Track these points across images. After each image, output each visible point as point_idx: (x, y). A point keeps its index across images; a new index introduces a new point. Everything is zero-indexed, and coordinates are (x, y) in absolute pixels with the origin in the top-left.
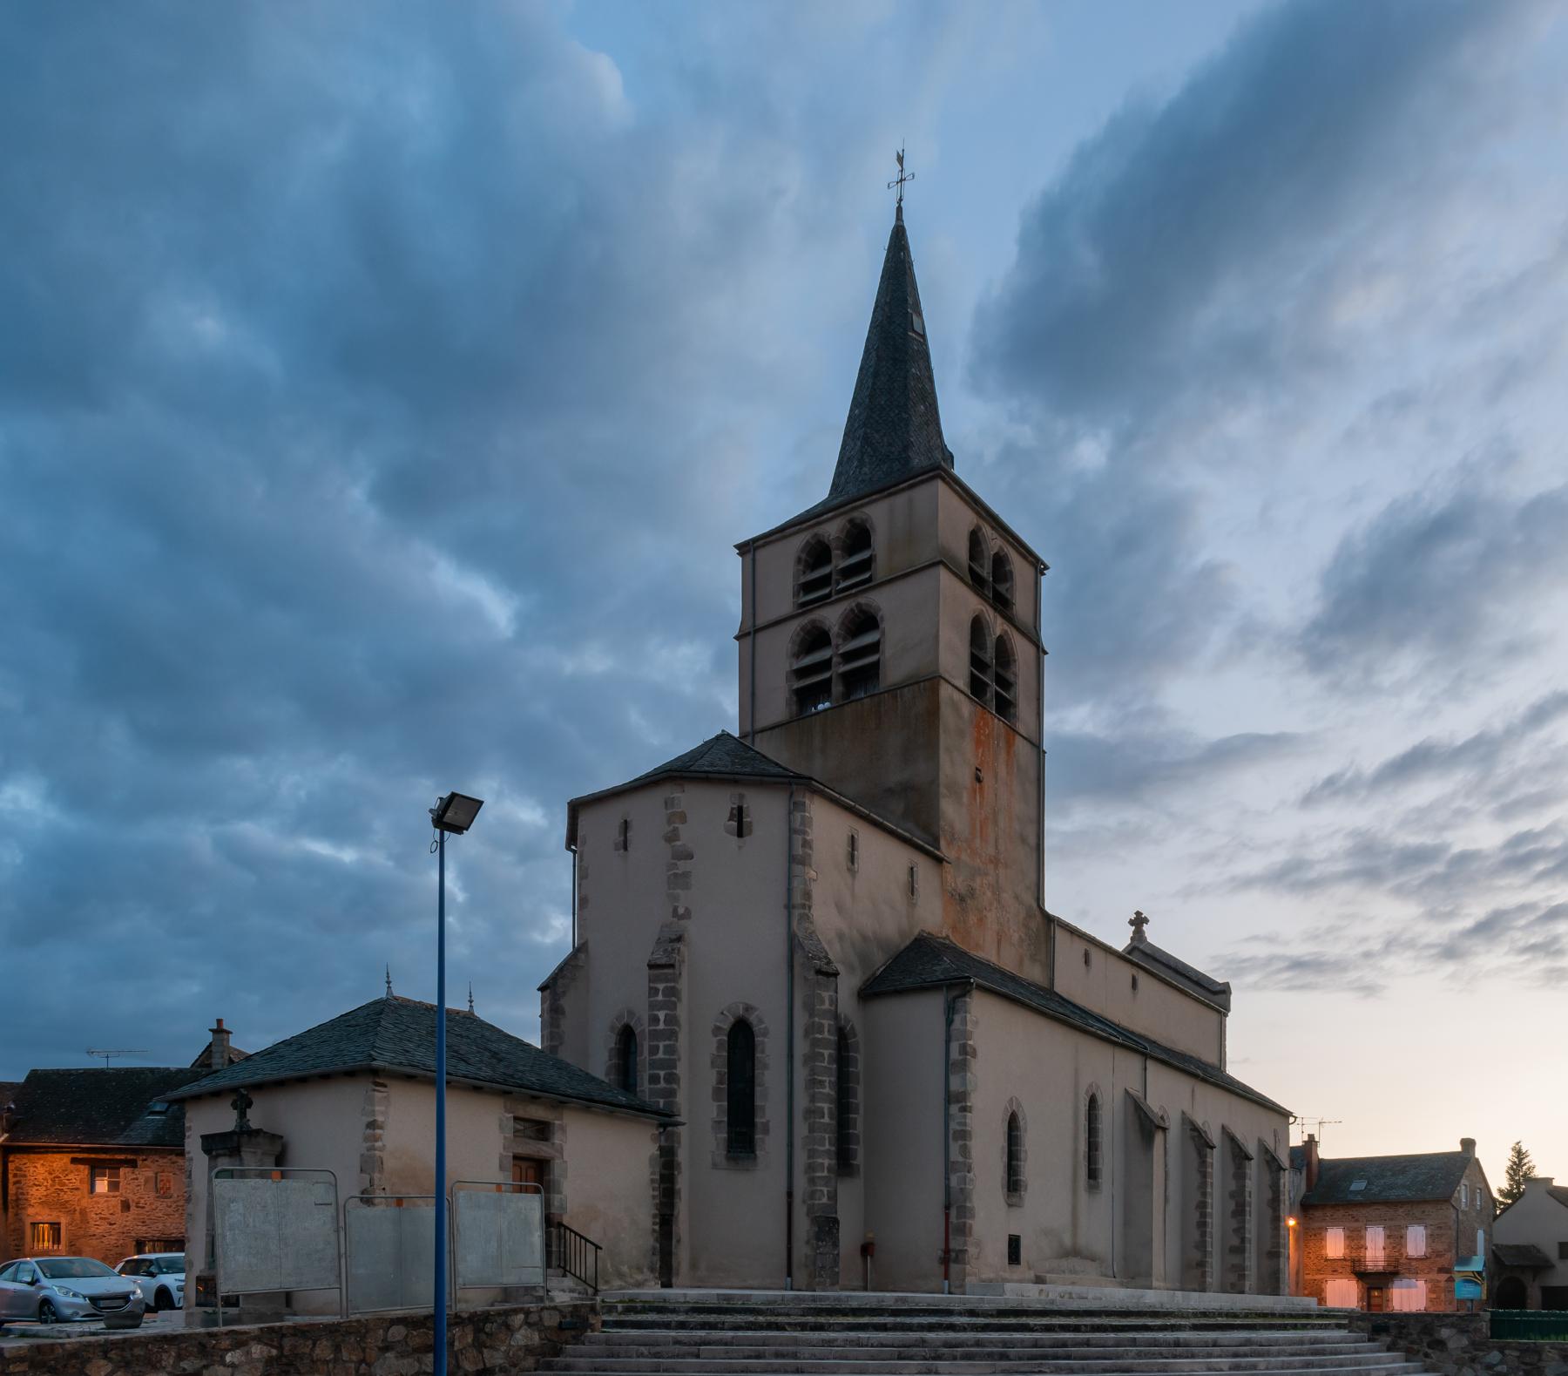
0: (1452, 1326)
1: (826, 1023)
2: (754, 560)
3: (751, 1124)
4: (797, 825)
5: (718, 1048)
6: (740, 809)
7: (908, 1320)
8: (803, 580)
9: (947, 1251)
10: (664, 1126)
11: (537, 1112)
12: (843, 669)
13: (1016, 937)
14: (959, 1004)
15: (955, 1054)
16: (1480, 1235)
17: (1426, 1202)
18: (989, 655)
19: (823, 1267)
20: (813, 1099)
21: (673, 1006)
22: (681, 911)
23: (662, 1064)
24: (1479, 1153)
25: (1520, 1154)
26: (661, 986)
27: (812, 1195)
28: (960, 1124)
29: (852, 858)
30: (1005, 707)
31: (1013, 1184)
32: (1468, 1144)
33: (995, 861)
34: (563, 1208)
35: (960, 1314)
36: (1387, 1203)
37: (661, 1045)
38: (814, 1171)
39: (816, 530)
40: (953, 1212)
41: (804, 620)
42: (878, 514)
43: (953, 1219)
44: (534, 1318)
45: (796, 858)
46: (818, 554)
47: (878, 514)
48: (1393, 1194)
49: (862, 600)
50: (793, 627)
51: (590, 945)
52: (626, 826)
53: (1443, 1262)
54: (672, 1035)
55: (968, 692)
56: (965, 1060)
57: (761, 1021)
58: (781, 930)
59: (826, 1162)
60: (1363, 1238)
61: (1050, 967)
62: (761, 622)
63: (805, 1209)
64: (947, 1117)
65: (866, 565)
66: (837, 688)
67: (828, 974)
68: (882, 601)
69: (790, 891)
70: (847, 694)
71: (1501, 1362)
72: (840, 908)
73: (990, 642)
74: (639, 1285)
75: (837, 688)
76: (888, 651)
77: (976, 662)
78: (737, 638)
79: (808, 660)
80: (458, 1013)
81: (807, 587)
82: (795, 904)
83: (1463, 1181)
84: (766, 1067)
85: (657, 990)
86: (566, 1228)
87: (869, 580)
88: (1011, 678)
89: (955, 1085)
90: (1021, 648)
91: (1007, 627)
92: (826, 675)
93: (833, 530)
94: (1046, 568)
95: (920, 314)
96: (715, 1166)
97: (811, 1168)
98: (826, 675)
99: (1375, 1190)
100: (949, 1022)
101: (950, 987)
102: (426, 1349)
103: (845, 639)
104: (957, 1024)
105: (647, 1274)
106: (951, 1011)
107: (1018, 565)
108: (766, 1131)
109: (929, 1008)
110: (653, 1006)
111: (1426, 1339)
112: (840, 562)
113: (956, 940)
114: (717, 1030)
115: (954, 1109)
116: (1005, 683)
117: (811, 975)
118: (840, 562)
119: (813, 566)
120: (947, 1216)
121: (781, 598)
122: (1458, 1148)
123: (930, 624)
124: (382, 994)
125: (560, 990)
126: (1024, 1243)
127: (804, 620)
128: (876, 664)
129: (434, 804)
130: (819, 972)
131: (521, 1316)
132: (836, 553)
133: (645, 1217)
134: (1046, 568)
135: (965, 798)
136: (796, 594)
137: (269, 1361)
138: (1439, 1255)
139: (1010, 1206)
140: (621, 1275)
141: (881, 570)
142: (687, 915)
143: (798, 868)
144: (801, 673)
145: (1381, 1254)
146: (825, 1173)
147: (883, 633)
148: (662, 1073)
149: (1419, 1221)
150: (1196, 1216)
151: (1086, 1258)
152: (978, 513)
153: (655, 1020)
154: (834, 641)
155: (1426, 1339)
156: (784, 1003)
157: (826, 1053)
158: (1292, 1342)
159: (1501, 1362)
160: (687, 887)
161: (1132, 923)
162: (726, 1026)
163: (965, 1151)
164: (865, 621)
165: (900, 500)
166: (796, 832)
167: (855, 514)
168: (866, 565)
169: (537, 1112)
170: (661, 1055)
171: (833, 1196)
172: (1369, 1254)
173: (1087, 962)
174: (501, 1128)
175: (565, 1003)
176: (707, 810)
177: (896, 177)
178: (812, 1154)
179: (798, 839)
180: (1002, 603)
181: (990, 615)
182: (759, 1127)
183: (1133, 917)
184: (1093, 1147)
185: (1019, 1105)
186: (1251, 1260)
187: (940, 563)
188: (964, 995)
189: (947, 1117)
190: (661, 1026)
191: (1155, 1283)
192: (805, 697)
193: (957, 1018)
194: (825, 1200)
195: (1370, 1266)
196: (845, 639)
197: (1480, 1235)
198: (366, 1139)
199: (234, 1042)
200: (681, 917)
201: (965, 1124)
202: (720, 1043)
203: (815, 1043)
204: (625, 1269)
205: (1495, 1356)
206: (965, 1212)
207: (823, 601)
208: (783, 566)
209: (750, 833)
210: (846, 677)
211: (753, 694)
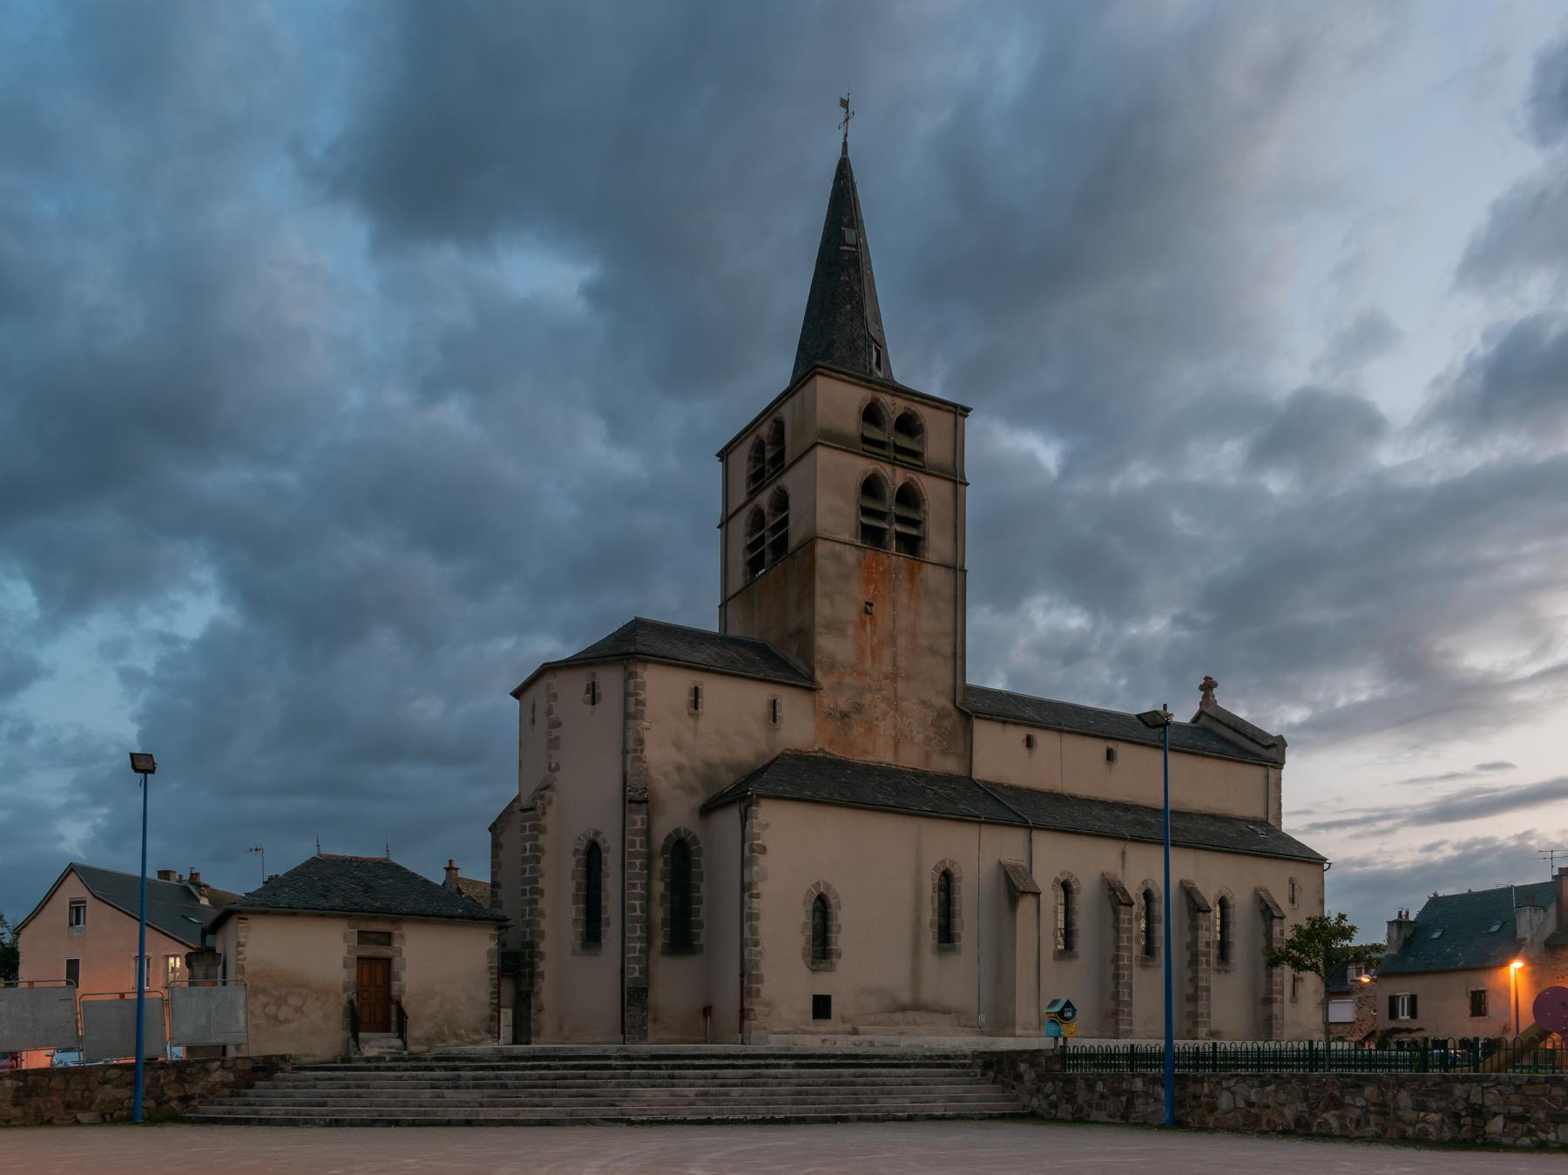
0: (1025, 1061)
1: (638, 839)
4: (631, 689)
10: (500, 928)
12: (899, 528)
13: (920, 738)
19: (633, 1027)
33: (893, 677)
34: (402, 991)
35: (616, 1058)
45: (631, 713)
64: (742, 902)
69: (625, 741)
72: (678, 746)
74: (476, 1043)
82: (631, 748)
90: (932, 489)
93: (765, 430)
100: (743, 828)
105: (484, 1035)
106: (744, 818)
108: (608, 924)
113: (837, 752)
114: (576, 852)
124: (315, 854)
135: (850, 630)
137: (18, 1089)
140: (457, 1036)
142: (557, 768)
143: (631, 722)
150: (1111, 969)
151: (935, 1011)
157: (638, 862)
161: (1201, 688)
162: (582, 848)
174: (345, 939)
175: (503, 840)
187: (817, 444)
189: (742, 902)
191: (1018, 1032)
192: (754, 564)
199: (460, 874)
202: (578, 861)
204: (462, 1032)
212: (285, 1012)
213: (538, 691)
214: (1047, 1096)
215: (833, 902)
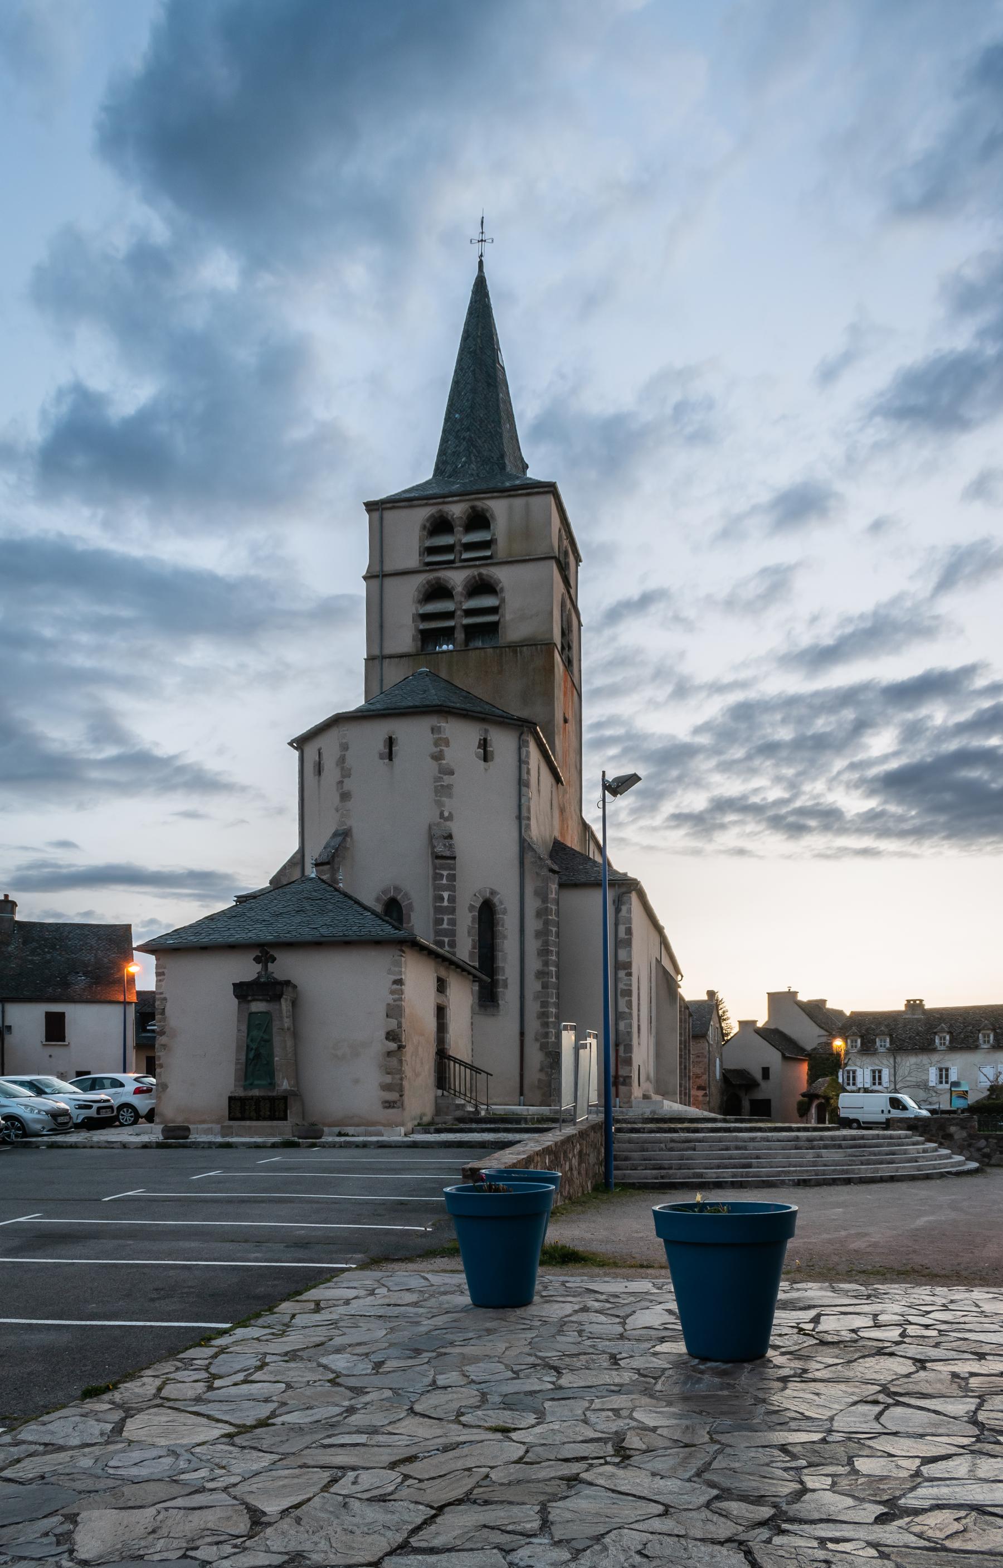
0: (957, 1125)
5: (473, 921)
6: (485, 740)
7: (700, 1125)
8: (428, 543)
12: (467, 621)
14: (625, 898)
22: (446, 814)
32: (711, 994)
37: (446, 918)
39: (440, 507)
40: (621, 1048)
41: (431, 576)
43: (621, 1053)
46: (440, 525)
49: (484, 571)
50: (420, 579)
51: (354, 831)
52: (391, 742)
54: (452, 910)
57: (501, 903)
58: (515, 835)
66: (460, 635)
68: (502, 575)
70: (467, 641)
71: (986, 1147)
76: (509, 615)
78: (365, 578)
79: (431, 608)
82: (522, 818)
85: (442, 876)
93: (457, 510)
104: (624, 912)
108: (506, 986)
111: (941, 1133)
114: (471, 908)
121: (407, 551)
122: (705, 997)
125: (336, 866)
127: (431, 576)
132: (459, 529)
142: (450, 818)
144: (425, 617)
148: (446, 940)
154: (457, 598)
155: (941, 1133)
158: (854, 1138)
159: (986, 1147)
160: (450, 796)
162: (478, 905)
167: (478, 503)
168: (486, 545)
170: (445, 926)
179: (524, 767)
186: (877, 1081)
192: (428, 638)
193: (624, 908)
194: (553, 1039)
198: (392, 992)
200: (447, 819)
202: (473, 918)
205: (982, 1143)
206: (629, 1048)
208: (409, 530)
209: (492, 759)
210: (467, 628)
211: (381, 626)
213: (329, 743)
214: (979, 1150)
215: (499, 908)
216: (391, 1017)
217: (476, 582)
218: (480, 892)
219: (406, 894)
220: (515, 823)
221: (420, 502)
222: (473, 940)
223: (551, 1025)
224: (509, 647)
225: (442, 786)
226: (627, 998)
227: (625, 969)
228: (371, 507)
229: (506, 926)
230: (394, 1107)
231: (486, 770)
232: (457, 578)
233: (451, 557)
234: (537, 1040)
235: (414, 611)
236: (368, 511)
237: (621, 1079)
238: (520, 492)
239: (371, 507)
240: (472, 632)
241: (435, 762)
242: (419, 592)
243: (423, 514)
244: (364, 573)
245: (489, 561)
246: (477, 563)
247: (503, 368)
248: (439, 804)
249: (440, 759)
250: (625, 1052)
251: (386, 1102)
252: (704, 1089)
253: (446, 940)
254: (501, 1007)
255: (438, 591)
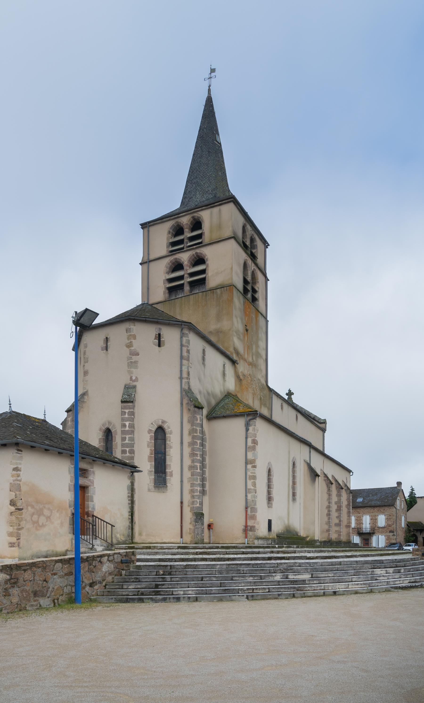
2: (149, 231)
3: (165, 473)
5: (150, 439)
6: (159, 335)
8: (171, 240)
9: (246, 526)
11: (83, 465)
15: (250, 443)
16: (403, 518)
17: (385, 506)
18: (249, 279)
20: (193, 461)
21: (133, 420)
22: (134, 378)
23: (127, 445)
24: (403, 487)
25: (412, 490)
26: (127, 411)
27: (193, 503)
28: (252, 473)
29: (204, 359)
30: (254, 299)
31: (270, 499)
32: (399, 484)
34: (94, 508)
36: (370, 507)
37: (127, 437)
38: (194, 492)
39: (177, 220)
40: (249, 510)
42: (206, 216)
44: (111, 558)
46: (179, 230)
47: (206, 216)
48: (373, 503)
49: (198, 251)
50: (167, 261)
51: (89, 392)
52: (107, 340)
53: (391, 528)
55: (243, 293)
56: (254, 446)
57: (169, 428)
59: (199, 489)
60: (362, 520)
61: (271, 410)
62: (152, 257)
63: (189, 509)
65: (200, 236)
66: (187, 288)
67: (201, 408)
73: (250, 273)
75: (187, 288)
77: (245, 281)
78: (141, 264)
80: (39, 419)
81: (173, 244)
83: (398, 498)
84: (171, 447)
85: (125, 412)
86: (96, 517)
87: (201, 243)
88: (257, 289)
89: (250, 456)
91: (255, 268)
92: (182, 282)
93: (185, 220)
94: (269, 245)
95: (219, 135)
96: (149, 490)
97: (192, 491)
98: (182, 282)
99: (366, 501)
100: (247, 430)
101: (248, 415)
102: (70, 574)
103: (190, 268)
106: (247, 426)
107: (259, 243)
108: (171, 475)
109: (237, 425)
110: (123, 420)
112: (188, 234)
115: (249, 466)
116: (254, 291)
117: (192, 408)
118: (188, 234)
119: (176, 235)
120: (246, 512)
123: (223, 263)
126: (273, 522)
127: (172, 258)
128: (204, 279)
129: (80, 310)
130: (195, 407)
131: (106, 557)
132: (186, 230)
133: (126, 514)
134: (269, 245)
136: (168, 247)
138: (390, 526)
139: (269, 507)
141: (206, 238)
142: (137, 380)
144: (171, 280)
145: (368, 526)
146: (198, 494)
147: (208, 266)
148: (128, 449)
149: (383, 513)
152: (245, 219)
153: (124, 426)
154: (185, 268)
156: (179, 420)
160: (136, 367)
162: (154, 429)
163: (254, 485)
164: (200, 260)
165: (215, 210)
166: (185, 346)
167: (195, 214)
168: (200, 236)
169: (83, 465)
170: (127, 441)
171: (201, 503)
172: (364, 526)
173: (282, 408)
176: (145, 333)
177: (208, 76)
178: (192, 485)
180: (253, 257)
181: (250, 262)
182: (168, 474)
183: (287, 392)
184: (294, 483)
185: (271, 465)
188: (254, 419)
190: (127, 428)
194: (198, 505)
195: (364, 531)
196: (190, 268)
197: (403, 518)
200: (134, 381)
201: (254, 473)
202: (151, 437)
203: (194, 437)
206: (254, 510)
207: (181, 250)
211: (148, 289)
212: (42, 520)
215: (167, 431)
216: (12, 491)
217: (195, 258)
218: (155, 422)
219: (114, 425)
220: (179, 381)
221: (167, 219)
222: (151, 450)
223: (196, 497)
224: (210, 290)
225: (131, 362)
226: (252, 481)
227: (251, 463)
228: (144, 226)
229: (172, 441)
230: (14, 546)
231: (159, 351)
232: (185, 257)
233: (181, 246)
234: (189, 506)
235: (164, 278)
236: (142, 228)
237: (249, 528)
238: (216, 204)
239: (144, 226)
240: (193, 284)
241: (128, 349)
242: (167, 267)
243: (168, 225)
244: (140, 262)
245: (200, 245)
246: (194, 247)
247: (220, 144)
248: (130, 372)
249: (130, 347)
250: (251, 512)
251: (11, 543)
252: (393, 532)
253: (128, 449)
254: (168, 488)
255: (178, 266)
